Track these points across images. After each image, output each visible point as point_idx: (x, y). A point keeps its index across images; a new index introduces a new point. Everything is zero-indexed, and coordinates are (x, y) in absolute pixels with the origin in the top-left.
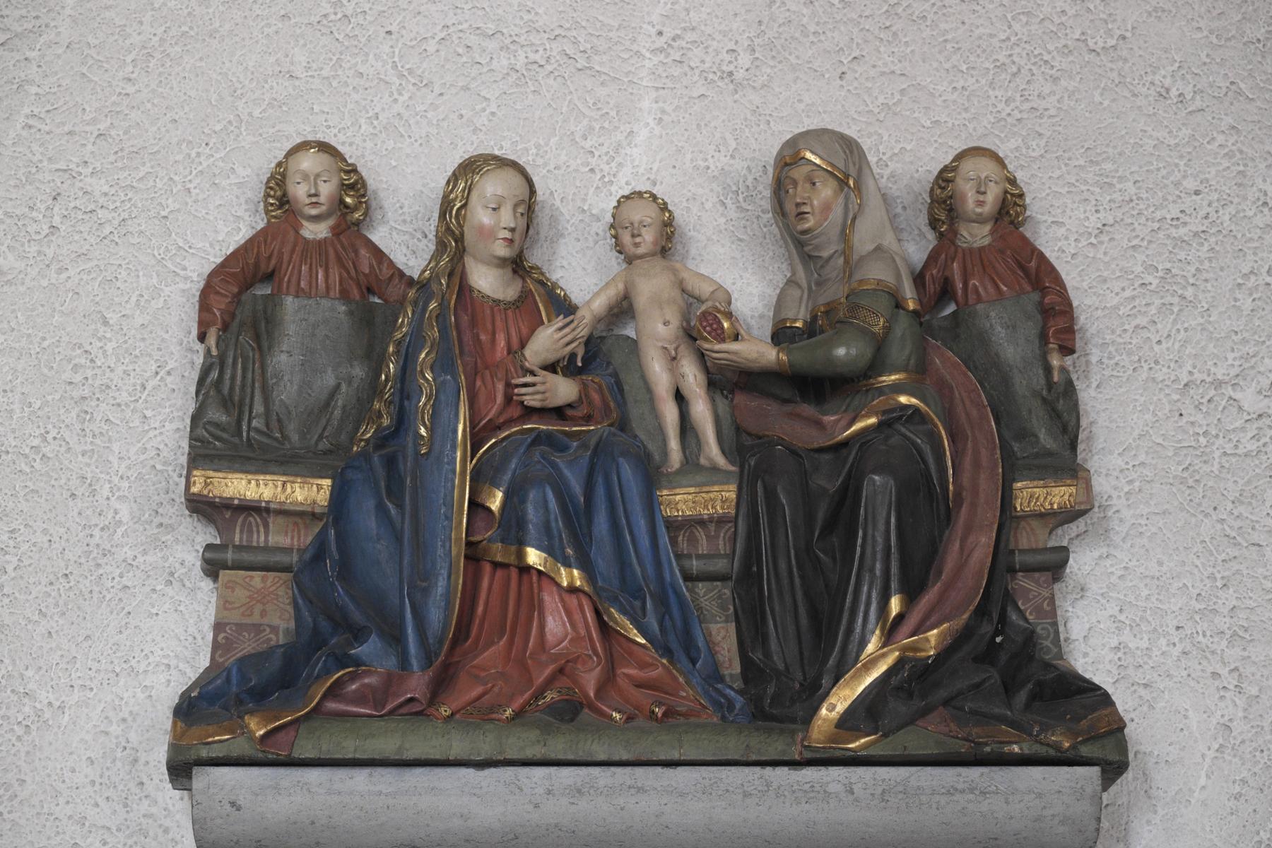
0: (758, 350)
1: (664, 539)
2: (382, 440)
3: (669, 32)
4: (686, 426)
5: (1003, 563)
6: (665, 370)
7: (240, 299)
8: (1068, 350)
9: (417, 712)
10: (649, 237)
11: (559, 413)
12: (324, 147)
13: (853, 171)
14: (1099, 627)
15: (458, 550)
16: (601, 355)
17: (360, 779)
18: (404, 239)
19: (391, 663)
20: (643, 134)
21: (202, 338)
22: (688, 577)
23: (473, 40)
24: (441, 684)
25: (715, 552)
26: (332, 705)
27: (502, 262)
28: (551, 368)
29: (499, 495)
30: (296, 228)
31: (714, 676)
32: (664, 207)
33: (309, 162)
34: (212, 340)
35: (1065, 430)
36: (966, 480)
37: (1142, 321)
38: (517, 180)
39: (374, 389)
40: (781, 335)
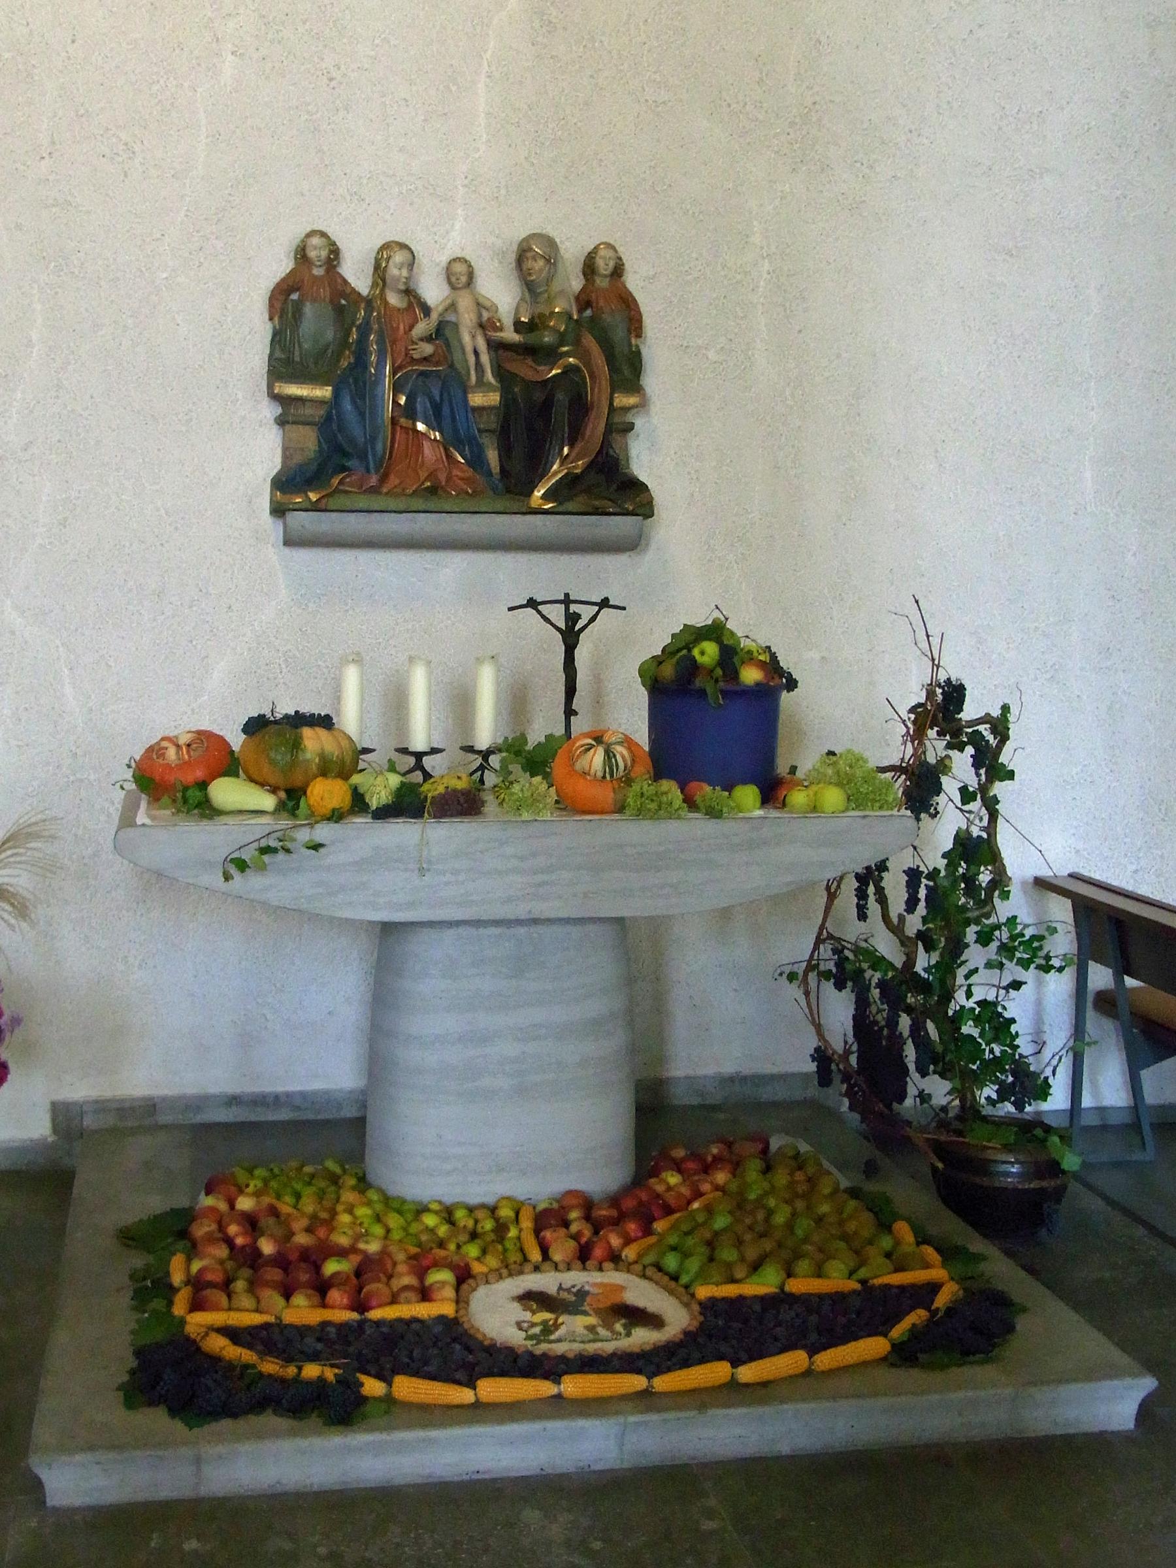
0: (510, 335)
1: (470, 415)
2: (352, 368)
3: (470, 177)
4: (478, 363)
5: (610, 429)
6: (470, 340)
7: (286, 301)
8: (639, 336)
9: (374, 491)
10: (464, 279)
11: (425, 359)
12: (323, 234)
13: (553, 255)
14: (644, 460)
15: (388, 422)
16: (442, 333)
17: (352, 517)
18: (356, 274)
19: (363, 470)
20: (457, 227)
21: (271, 319)
22: (479, 431)
23: (382, 178)
24: (384, 479)
25: (492, 422)
26: (341, 487)
27: (400, 291)
28: (422, 340)
29: (404, 398)
30: (310, 270)
31: (490, 474)
32: (470, 266)
33: (316, 241)
34: (276, 319)
35: (635, 369)
36: (595, 398)
37: (670, 319)
38: (410, 256)
39: (344, 343)
40: (518, 326)
